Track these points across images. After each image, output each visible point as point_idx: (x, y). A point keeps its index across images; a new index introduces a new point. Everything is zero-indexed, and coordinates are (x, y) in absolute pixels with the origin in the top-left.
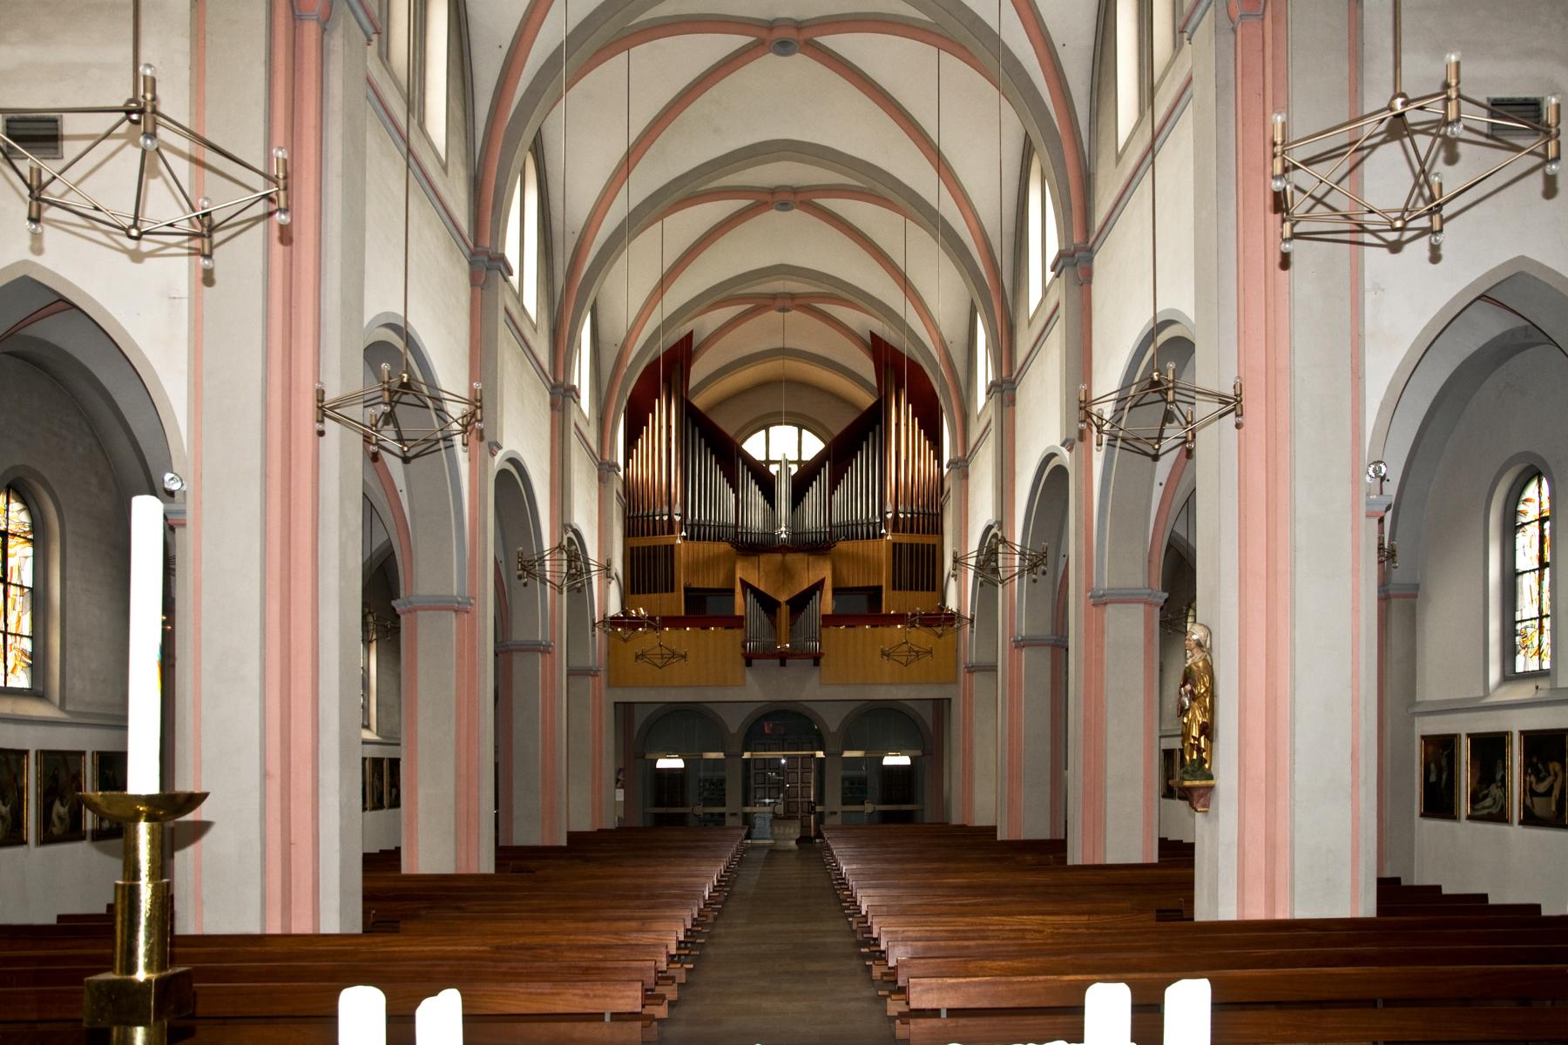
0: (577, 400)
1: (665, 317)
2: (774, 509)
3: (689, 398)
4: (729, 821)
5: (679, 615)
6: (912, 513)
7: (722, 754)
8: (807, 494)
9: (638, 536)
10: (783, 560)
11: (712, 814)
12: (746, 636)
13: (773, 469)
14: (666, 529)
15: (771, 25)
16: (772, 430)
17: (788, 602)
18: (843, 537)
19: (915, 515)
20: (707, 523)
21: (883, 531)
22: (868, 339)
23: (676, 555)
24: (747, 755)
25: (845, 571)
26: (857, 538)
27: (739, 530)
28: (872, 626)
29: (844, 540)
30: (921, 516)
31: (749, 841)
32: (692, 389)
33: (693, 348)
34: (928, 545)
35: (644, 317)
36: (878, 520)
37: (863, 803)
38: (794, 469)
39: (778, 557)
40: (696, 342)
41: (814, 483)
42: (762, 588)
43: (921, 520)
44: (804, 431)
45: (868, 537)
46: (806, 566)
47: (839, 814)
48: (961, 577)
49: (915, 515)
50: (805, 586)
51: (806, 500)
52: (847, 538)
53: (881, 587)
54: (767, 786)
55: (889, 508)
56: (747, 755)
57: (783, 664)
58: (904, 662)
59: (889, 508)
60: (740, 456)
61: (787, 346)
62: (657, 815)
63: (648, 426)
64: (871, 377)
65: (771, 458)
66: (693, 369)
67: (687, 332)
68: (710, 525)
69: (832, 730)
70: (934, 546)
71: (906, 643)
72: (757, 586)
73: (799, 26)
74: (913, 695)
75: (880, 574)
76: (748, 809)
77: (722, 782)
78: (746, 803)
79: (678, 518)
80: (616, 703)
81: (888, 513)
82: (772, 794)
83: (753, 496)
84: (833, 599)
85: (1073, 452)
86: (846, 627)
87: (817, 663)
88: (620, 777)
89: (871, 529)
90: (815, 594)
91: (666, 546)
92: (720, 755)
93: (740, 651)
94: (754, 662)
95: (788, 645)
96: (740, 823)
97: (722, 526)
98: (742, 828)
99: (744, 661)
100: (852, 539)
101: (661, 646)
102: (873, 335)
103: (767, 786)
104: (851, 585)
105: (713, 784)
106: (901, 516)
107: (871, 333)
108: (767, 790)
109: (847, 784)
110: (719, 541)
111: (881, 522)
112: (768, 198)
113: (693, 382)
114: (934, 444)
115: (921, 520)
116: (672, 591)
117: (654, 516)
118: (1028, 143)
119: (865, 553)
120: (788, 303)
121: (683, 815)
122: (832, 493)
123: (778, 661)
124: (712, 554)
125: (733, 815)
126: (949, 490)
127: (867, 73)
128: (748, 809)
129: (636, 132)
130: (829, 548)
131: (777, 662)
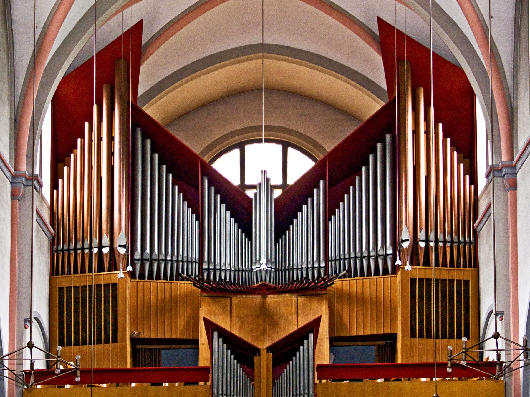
2: (250, 239)
9: (69, 273)
22: (375, 28)
27: (205, 266)
39: (257, 299)
55: (406, 234)
63: (83, 137)
70: (467, 282)
75: (394, 320)
89: (380, 262)
90: (308, 338)
104: (354, 333)
116: (115, 341)
122: (328, 218)
124: (167, 295)
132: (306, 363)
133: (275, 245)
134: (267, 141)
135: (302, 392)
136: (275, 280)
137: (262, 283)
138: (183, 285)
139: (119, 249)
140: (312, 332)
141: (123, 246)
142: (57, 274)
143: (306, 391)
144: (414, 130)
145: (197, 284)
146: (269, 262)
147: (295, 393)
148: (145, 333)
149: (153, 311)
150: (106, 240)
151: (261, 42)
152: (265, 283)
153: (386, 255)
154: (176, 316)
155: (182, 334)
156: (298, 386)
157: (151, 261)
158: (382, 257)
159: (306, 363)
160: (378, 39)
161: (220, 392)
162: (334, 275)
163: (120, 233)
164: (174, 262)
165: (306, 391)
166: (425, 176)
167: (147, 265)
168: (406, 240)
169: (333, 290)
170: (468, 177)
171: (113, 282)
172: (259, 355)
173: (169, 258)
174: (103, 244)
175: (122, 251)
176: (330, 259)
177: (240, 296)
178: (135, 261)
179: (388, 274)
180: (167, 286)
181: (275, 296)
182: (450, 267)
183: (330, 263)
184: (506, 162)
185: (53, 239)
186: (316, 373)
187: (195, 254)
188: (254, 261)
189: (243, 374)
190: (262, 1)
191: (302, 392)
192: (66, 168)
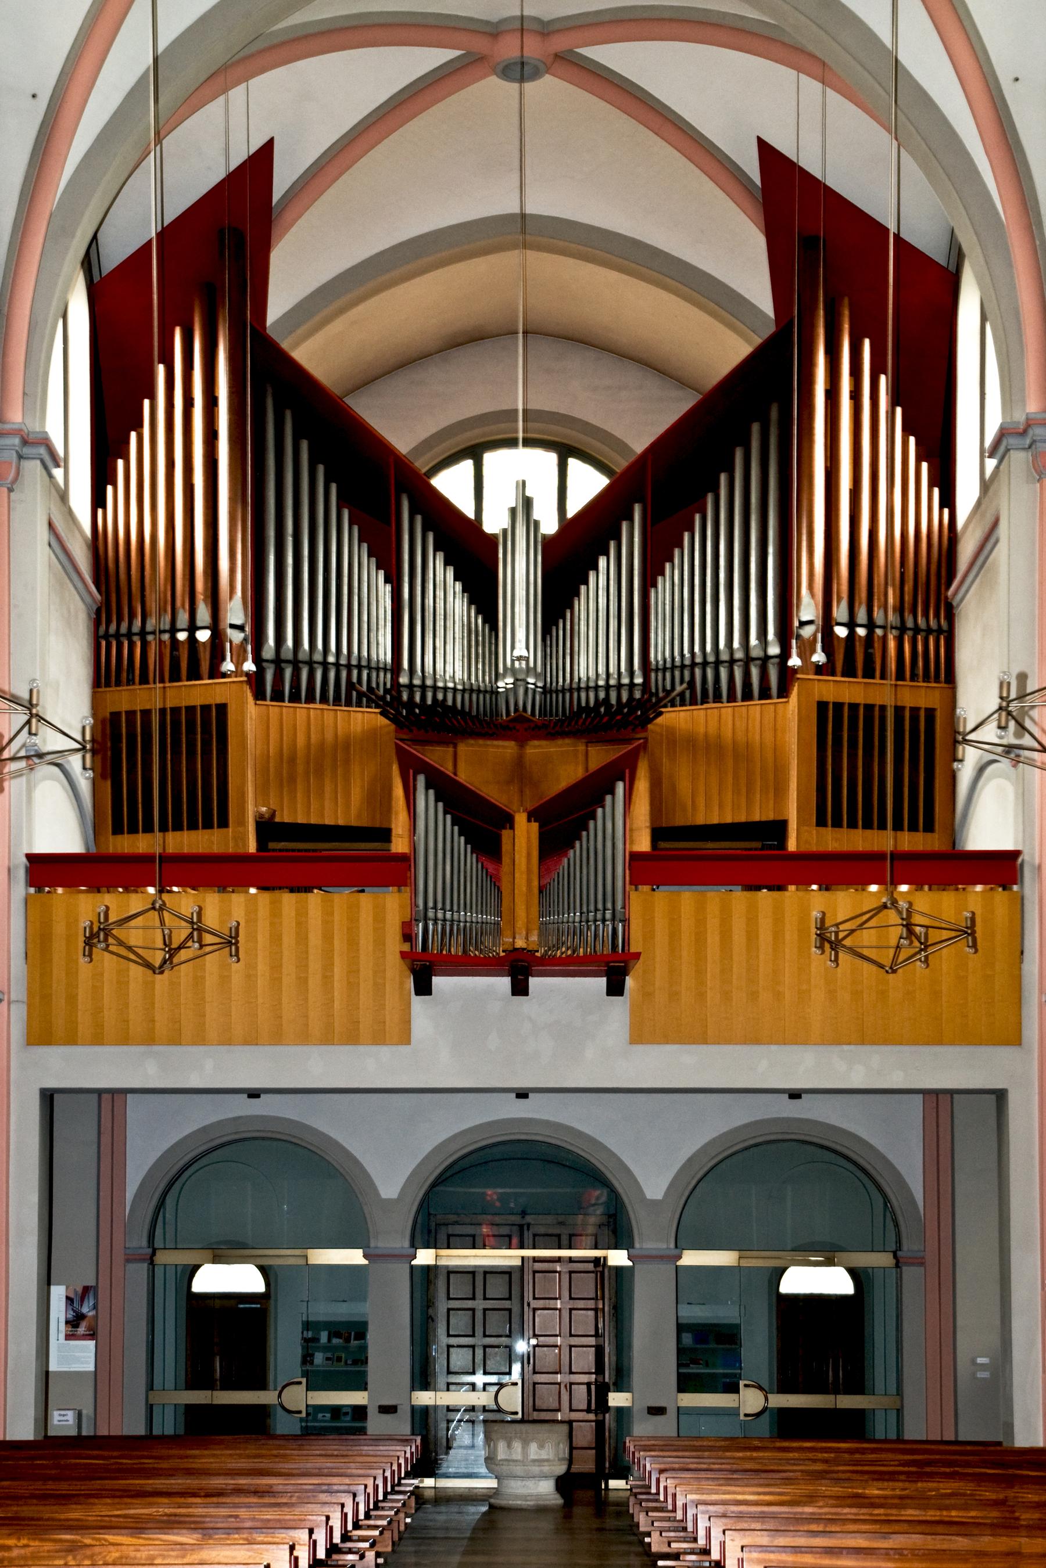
2: (494, 628)
4: (375, 1423)
6: (871, 626)
7: (359, 1253)
9: (130, 681)
11: (336, 1411)
15: (494, 31)
16: (489, 458)
20: (318, 657)
22: (751, 166)
24: (425, 1257)
25: (684, 786)
27: (404, 680)
31: (429, 1482)
34: (915, 710)
36: (774, 650)
37: (733, 1389)
39: (506, 748)
40: (282, 179)
41: (602, 562)
44: (573, 463)
45: (747, 696)
47: (672, 1413)
51: (580, 605)
54: (479, 1341)
55: (808, 609)
56: (425, 1257)
57: (520, 989)
58: (887, 962)
62: (190, 1409)
63: (153, 398)
69: (649, 1195)
70: (930, 713)
73: (546, 29)
75: (780, 790)
76: (424, 1398)
77: (358, 1330)
78: (423, 1379)
81: (803, 624)
82: (491, 1365)
83: (440, 593)
88: (85, 1310)
89: (755, 672)
90: (612, 792)
91: (206, 708)
92: (355, 1257)
96: (406, 1429)
98: (405, 1441)
103: (479, 1304)
104: (701, 820)
105: (338, 1335)
108: (479, 1352)
109: (688, 1339)
116: (224, 823)
118: (954, 253)
121: (262, 1412)
122: (649, 582)
124: (329, 736)
125: (388, 1410)
128: (424, 1398)
132: (609, 844)
133: (544, 640)
134: (528, 443)
135: (600, 906)
136: (543, 711)
137: (517, 714)
138: (360, 715)
139: (229, 631)
140: (623, 780)
141: (240, 628)
142: (108, 684)
143: (609, 905)
144: (829, 388)
145: (385, 684)
146: (532, 672)
147: (585, 910)
148: (285, 812)
149: (300, 768)
150: (203, 614)
151: (517, 211)
152: (524, 714)
153: (767, 658)
154: (347, 780)
155: (359, 816)
156: (592, 879)
157: (296, 663)
158: (759, 662)
159: (609, 844)
160: (759, 196)
161: (431, 904)
162: (661, 694)
163: (231, 598)
164: (341, 668)
165: (609, 905)
166: (850, 490)
167: (288, 673)
168: (810, 622)
169: (658, 729)
170: (936, 491)
171: (218, 701)
172: (512, 827)
173: (331, 659)
174: (199, 623)
175: (237, 637)
176: (653, 667)
177: (472, 742)
178: (265, 664)
179: (769, 697)
180: (329, 716)
181: (544, 743)
182: (897, 679)
183: (653, 675)
184: (1035, 413)
185: (98, 612)
186: (627, 872)
187: (384, 653)
188: (501, 670)
189: (477, 867)
190: (519, 3)
191: (600, 906)
192: (120, 463)
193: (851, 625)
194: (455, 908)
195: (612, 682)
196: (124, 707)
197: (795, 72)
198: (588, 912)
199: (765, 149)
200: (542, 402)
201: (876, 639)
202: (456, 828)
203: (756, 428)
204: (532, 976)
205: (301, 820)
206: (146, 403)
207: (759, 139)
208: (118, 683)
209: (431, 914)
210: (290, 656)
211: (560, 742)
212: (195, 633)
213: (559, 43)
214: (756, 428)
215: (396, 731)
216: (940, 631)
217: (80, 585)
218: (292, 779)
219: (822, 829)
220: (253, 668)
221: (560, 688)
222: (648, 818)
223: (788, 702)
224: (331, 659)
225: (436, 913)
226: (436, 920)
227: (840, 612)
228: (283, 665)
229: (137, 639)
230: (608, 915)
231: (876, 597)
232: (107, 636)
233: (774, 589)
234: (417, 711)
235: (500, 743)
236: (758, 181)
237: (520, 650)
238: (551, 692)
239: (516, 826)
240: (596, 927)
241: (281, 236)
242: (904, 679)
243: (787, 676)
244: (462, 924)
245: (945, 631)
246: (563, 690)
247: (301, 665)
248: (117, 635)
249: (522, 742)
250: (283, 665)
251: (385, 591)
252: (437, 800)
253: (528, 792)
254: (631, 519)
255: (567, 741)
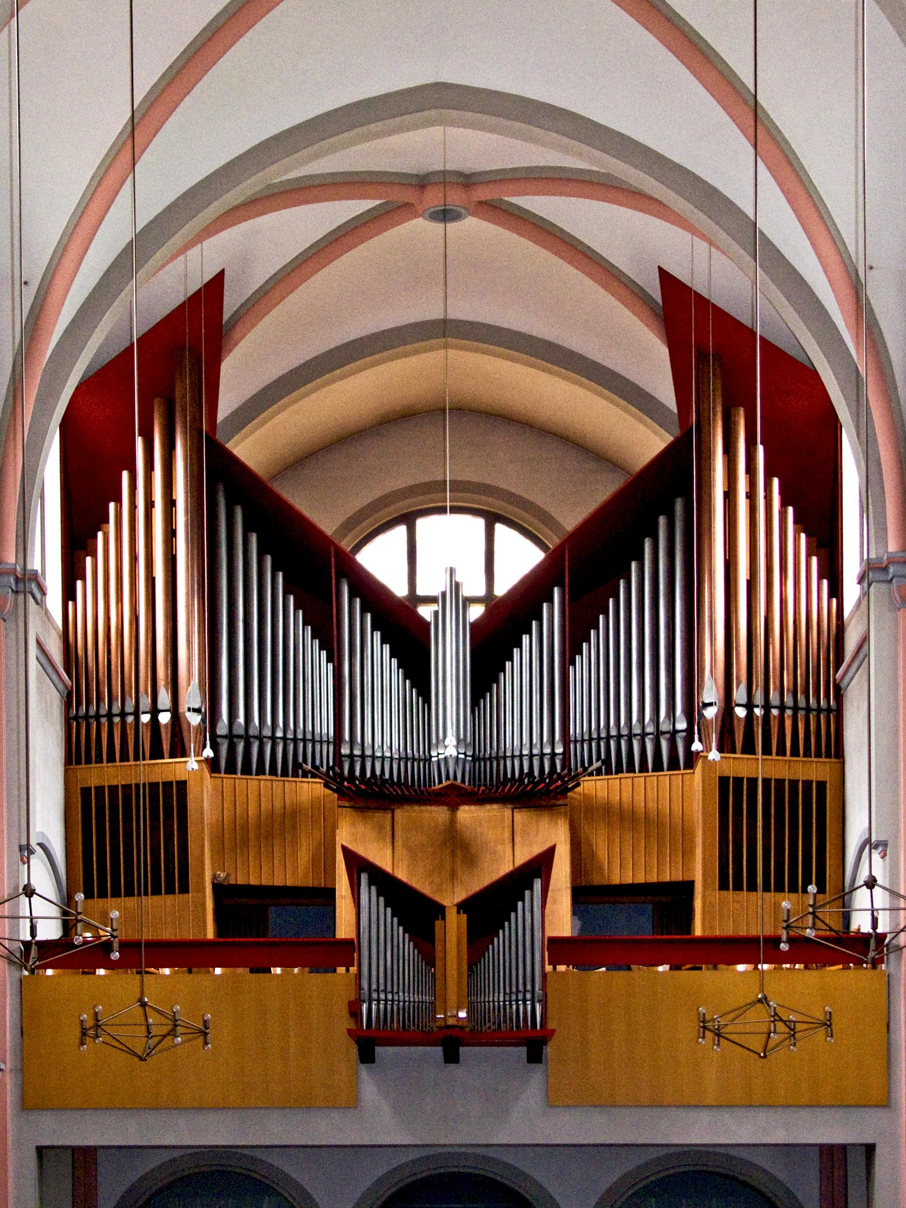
0: (38, 596)
1: (142, 222)
3: (219, 436)
5: (200, 937)
6: (767, 707)
8: (508, 664)
9: (99, 760)
10: (453, 820)
12: (359, 987)
13: (426, 612)
14: (166, 746)
16: (422, 524)
17: (462, 907)
18: (596, 765)
19: (775, 712)
21: (697, 746)
22: (655, 291)
23: (191, 806)
25: (602, 853)
26: (631, 769)
27: (345, 750)
28: (675, 967)
29: (599, 772)
30: (789, 712)
32: (226, 419)
33: (226, 316)
34: (808, 784)
35: (95, 207)
36: (682, 725)
38: (476, 612)
39: (438, 814)
40: (231, 303)
41: (525, 639)
42: (401, 874)
43: (788, 723)
44: (500, 528)
45: (658, 767)
46: (507, 834)
48: (896, 847)
49: (775, 712)
50: (506, 868)
52: (607, 768)
53: (691, 885)
55: (711, 692)
57: (452, 1057)
59: (711, 692)
60: (344, 575)
61: (452, 315)
64: (666, 394)
65: (421, 591)
66: (228, 367)
67: (207, 278)
68: (273, 738)
70: (821, 785)
71: (764, 1000)
72: (389, 869)
74: (780, 1136)
75: (687, 853)
79: (195, 720)
80: (41, 1150)
84: (574, 913)
85: (887, 858)
86: (607, 970)
87: (535, 1056)
89: (664, 744)
93: (347, 1023)
94: (381, 1051)
95: (462, 1014)
97: (304, 740)
99: (354, 1051)
100: (619, 770)
101: (144, 1005)
102: (666, 278)
104: (616, 880)
106: (741, 712)
107: (662, 271)
110: (295, 775)
111: (689, 731)
112: (408, 196)
113: (226, 406)
114: (820, 545)
115: (788, 723)
116: (184, 889)
117: (137, 714)
119: (652, 805)
120: (455, 198)
122: (568, 660)
123: (438, 1051)
124: (278, 805)
126: (865, 639)
127: (582, 239)
129: (145, 84)
130: (564, 791)
131: (437, 1052)
133: (473, 712)
134: (455, 510)
135: (521, 988)
136: (473, 779)
138: (306, 785)
139: (188, 714)
142: (79, 762)
143: (529, 987)
149: (252, 835)
150: (165, 699)
155: (306, 876)
157: (247, 739)
161: (374, 987)
164: (289, 741)
165: (529, 987)
168: (711, 704)
170: (825, 582)
172: (444, 918)
173: (279, 734)
176: (572, 738)
178: (219, 740)
181: (473, 808)
183: (572, 746)
185: (69, 694)
187: (326, 728)
188: (434, 741)
191: (521, 988)
192: (89, 560)
193: (749, 706)
194: (395, 990)
195: (536, 751)
196: (93, 782)
197: (690, 235)
198: (511, 992)
199: (665, 276)
200: (470, 475)
201: (772, 719)
202: (395, 919)
203: (662, 520)
204: (462, 1046)
205: (253, 881)
206: (112, 506)
207: (660, 269)
208: (88, 761)
209: (375, 995)
210: (242, 732)
211: (488, 807)
212: (157, 716)
213: (482, 193)
214: (662, 520)
215: (339, 799)
216: (829, 710)
217: (54, 677)
218: (245, 842)
219: (724, 893)
220: (211, 754)
221: (487, 756)
222: (568, 880)
223: (694, 773)
224: (279, 734)
225: (379, 995)
226: (378, 1001)
227: (740, 694)
228: (235, 740)
229: (104, 720)
230: (528, 996)
231: (771, 680)
232: (76, 718)
233: (682, 667)
234: (357, 782)
235: (434, 808)
236: (659, 300)
237: (451, 751)
238: (479, 759)
239: (447, 918)
240: (518, 1006)
241: (230, 350)
242: (798, 756)
243: (691, 759)
244: (401, 1004)
245: (834, 710)
246: (490, 758)
247: (251, 740)
248: (87, 717)
249: (454, 808)
250: (235, 740)
251: (327, 669)
252: (379, 895)
253: (459, 853)
254: (551, 601)
255: (495, 806)
